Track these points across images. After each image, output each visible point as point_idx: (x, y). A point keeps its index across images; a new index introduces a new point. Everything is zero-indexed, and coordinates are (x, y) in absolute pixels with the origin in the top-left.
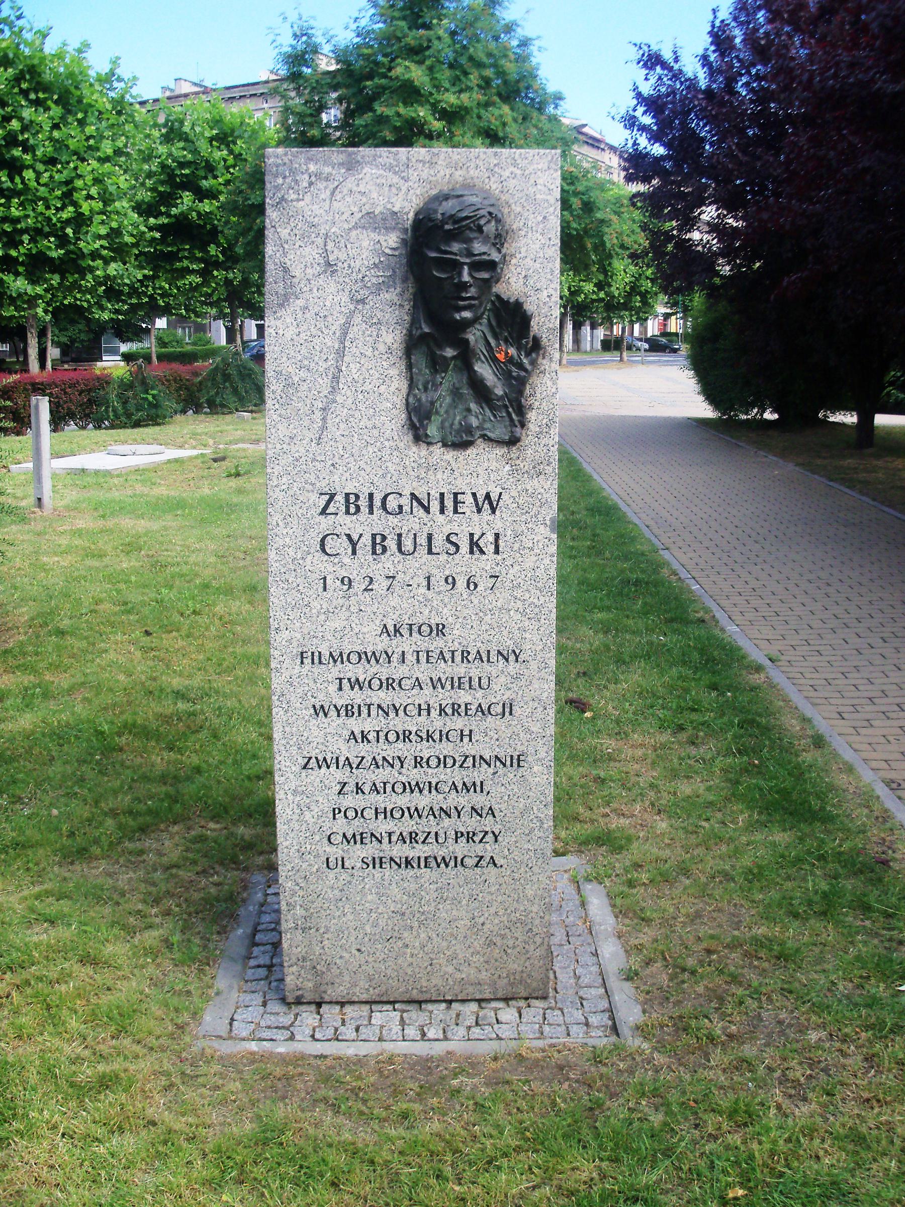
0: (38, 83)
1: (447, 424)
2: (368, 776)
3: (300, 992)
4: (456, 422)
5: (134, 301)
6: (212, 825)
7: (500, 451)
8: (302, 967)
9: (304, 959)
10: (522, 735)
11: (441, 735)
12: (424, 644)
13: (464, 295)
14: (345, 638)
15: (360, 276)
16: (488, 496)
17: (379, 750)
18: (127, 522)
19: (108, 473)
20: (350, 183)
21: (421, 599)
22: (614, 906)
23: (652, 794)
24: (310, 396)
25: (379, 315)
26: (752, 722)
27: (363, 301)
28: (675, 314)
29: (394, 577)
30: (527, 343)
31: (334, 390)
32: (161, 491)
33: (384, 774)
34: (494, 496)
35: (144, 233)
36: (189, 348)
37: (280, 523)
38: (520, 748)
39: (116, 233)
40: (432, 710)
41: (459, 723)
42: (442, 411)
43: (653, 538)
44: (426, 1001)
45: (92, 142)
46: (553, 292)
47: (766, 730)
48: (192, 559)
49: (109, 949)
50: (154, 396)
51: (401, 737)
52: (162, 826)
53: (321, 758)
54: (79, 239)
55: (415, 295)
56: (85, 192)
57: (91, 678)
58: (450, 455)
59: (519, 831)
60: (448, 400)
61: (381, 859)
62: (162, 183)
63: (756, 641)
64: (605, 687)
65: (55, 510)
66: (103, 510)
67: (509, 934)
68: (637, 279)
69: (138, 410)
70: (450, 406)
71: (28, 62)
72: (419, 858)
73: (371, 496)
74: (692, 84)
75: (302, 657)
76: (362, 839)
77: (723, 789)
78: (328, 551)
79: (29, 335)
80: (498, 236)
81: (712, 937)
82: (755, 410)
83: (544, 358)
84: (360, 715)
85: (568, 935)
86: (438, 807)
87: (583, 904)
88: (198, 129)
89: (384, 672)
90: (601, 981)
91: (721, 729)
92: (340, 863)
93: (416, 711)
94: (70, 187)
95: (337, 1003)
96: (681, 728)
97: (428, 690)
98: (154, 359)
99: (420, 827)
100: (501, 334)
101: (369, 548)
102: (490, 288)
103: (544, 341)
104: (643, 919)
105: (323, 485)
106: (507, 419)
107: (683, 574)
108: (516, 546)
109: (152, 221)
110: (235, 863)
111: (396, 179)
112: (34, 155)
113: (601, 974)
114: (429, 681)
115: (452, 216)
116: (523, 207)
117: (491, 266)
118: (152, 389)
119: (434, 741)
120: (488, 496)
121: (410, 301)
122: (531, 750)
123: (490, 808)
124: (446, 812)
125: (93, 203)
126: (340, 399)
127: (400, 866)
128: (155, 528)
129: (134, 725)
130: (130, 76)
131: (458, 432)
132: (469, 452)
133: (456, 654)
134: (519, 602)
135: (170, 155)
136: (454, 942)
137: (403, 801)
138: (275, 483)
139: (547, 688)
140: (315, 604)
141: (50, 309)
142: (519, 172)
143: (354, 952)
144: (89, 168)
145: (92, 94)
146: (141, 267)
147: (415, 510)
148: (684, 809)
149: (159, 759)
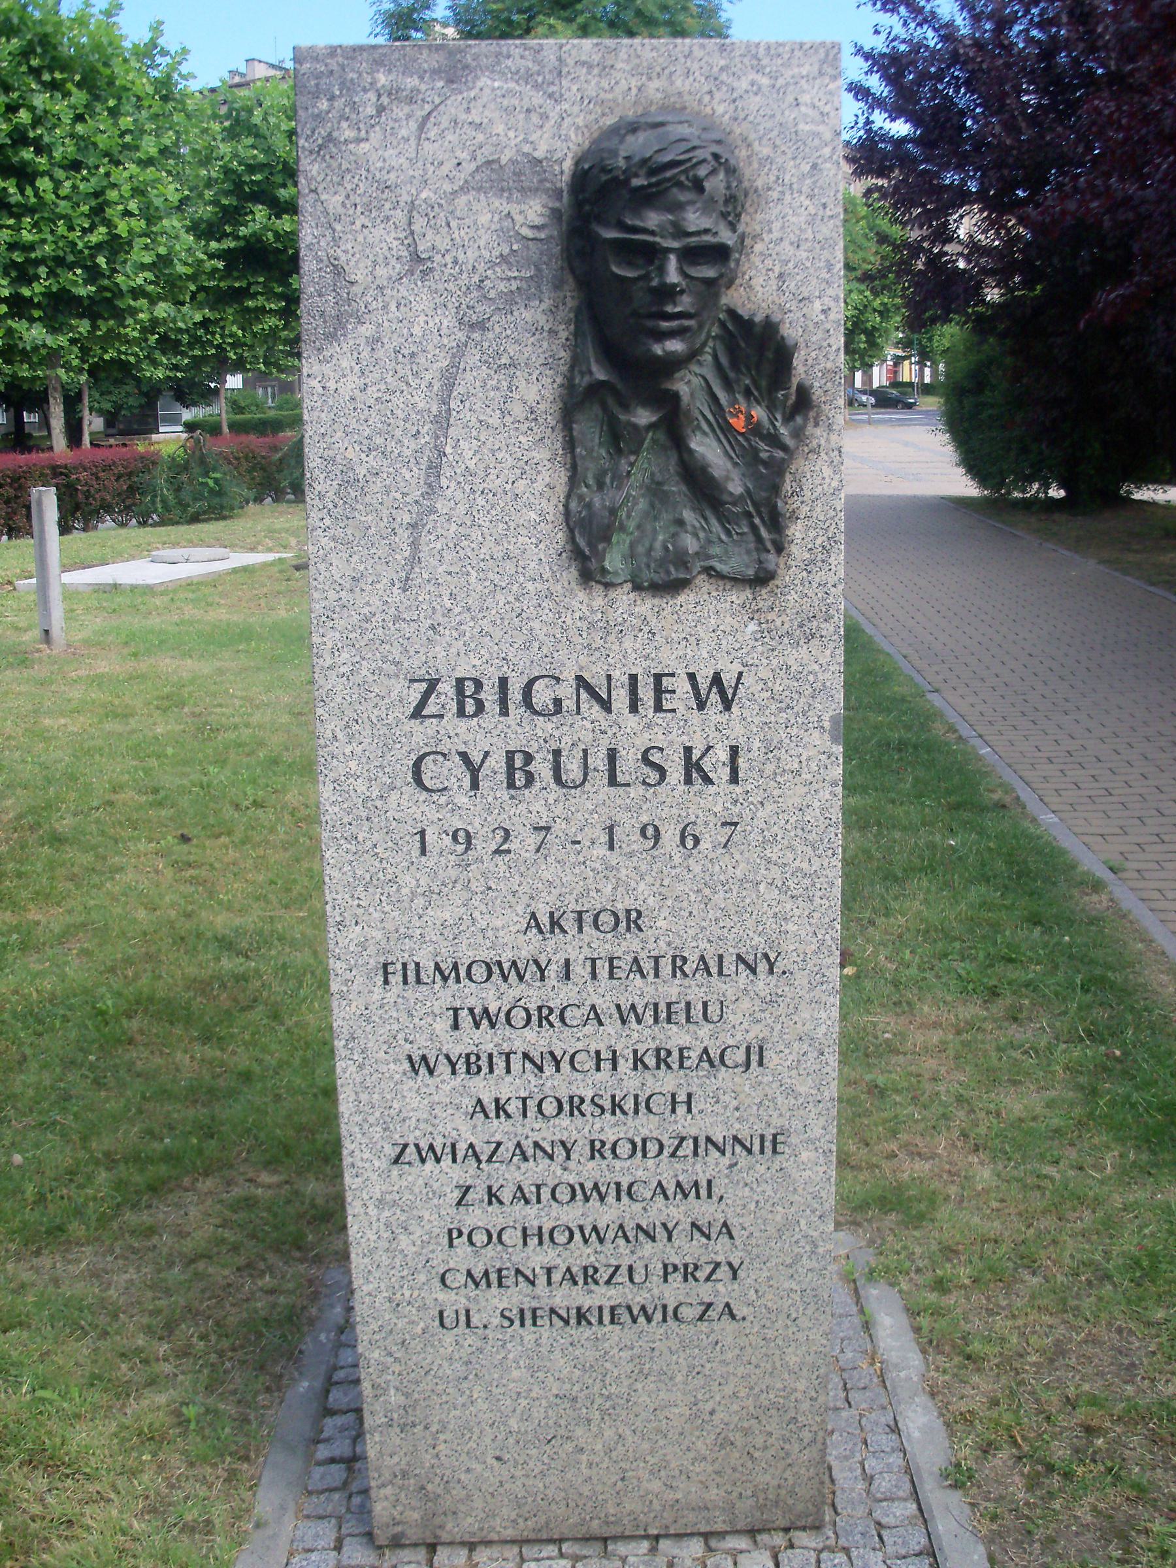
0: (53, 58)
1: (640, 549)
2: (508, 1176)
3: (399, 1529)
4: (658, 545)
5: (197, 352)
6: (266, 1178)
7: (739, 597)
8: (401, 1488)
9: (404, 1475)
10: (780, 1100)
11: (636, 1104)
12: (602, 944)
13: (670, 309)
14: (463, 937)
15: (476, 279)
16: (717, 680)
17: (527, 1131)
18: (167, 664)
19: (149, 590)
20: (453, 107)
21: (597, 866)
22: (917, 1330)
23: (961, 1114)
24: (388, 501)
25: (512, 349)
26: (1101, 981)
27: (481, 326)
28: (909, 357)
29: (548, 829)
30: (786, 397)
31: (432, 489)
32: (221, 614)
33: (538, 1170)
34: (728, 679)
35: (202, 261)
36: (272, 414)
37: (340, 736)
38: (777, 1122)
39: (163, 261)
40: (621, 1061)
41: (668, 1082)
42: (631, 525)
43: (914, 674)
44: (615, 1538)
45: (128, 138)
46: (832, 304)
47: (1124, 992)
48: (257, 718)
49: (80, 1436)
50: (216, 481)
51: (566, 1107)
52: (186, 1181)
53: (424, 1145)
54: (115, 271)
55: (578, 312)
56: (120, 207)
57: (94, 915)
58: (646, 605)
59: (774, 1261)
60: (642, 504)
61: (534, 1311)
62: (227, 193)
63: (1086, 839)
64: (872, 923)
65: (69, 646)
66: (138, 645)
67: (757, 1428)
68: (861, 312)
69: (195, 499)
70: (646, 514)
71: (39, 29)
72: (600, 1308)
73: (503, 682)
74: (948, 33)
75: (386, 973)
76: (500, 1278)
77: (1072, 1105)
78: (427, 783)
79: (51, 400)
80: (731, 199)
81: (1093, 1401)
82: (1036, 486)
83: (816, 425)
84: (491, 1071)
85: (845, 1389)
86: (633, 1224)
87: (867, 1326)
88: (272, 120)
89: (533, 995)
90: (908, 1486)
91: (1056, 994)
92: (463, 1318)
93: (592, 1064)
94: (100, 200)
95: (463, 1544)
96: (994, 993)
97: (612, 1027)
98: (226, 429)
99: (602, 1257)
100: (738, 381)
101: (502, 777)
102: (717, 296)
103: (817, 394)
104: (969, 1357)
105: (414, 664)
106: (751, 538)
107: (965, 731)
108: (770, 768)
109: (214, 245)
110: (299, 1248)
111: (538, 98)
112: (51, 157)
113: (908, 1470)
114: (614, 1010)
115: (645, 161)
116: (775, 146)
117: (720, 254)
118: (214, 470)
119: (624, 1113)
120: (717, 680)
121: (568, 323)
122: (797, 1124)
123: (725, 1224)
124: (646, 1233)
125: (134, 222)
126: (442, 506)
127: (567, 1322)
128: (206, 671)
129: (151, 1000)
130: (178, 48)
131: (662, 563)
132: (681, 598)
133: (662, 962)
134: (774, 869)
135: (235, 155)
136: (661, 1442)
137: (572, 1214)
138: (329, 662)
139: (825, 1019)
140: (407, 879)
141: (86, 367)
142: (765, 81)
143: (491, 1461)
144: (126, 174)
145: (127, 72)
146: (200, 307)
147: (584, 707)
148: (1013, 1143)
149: (187, 1060)
